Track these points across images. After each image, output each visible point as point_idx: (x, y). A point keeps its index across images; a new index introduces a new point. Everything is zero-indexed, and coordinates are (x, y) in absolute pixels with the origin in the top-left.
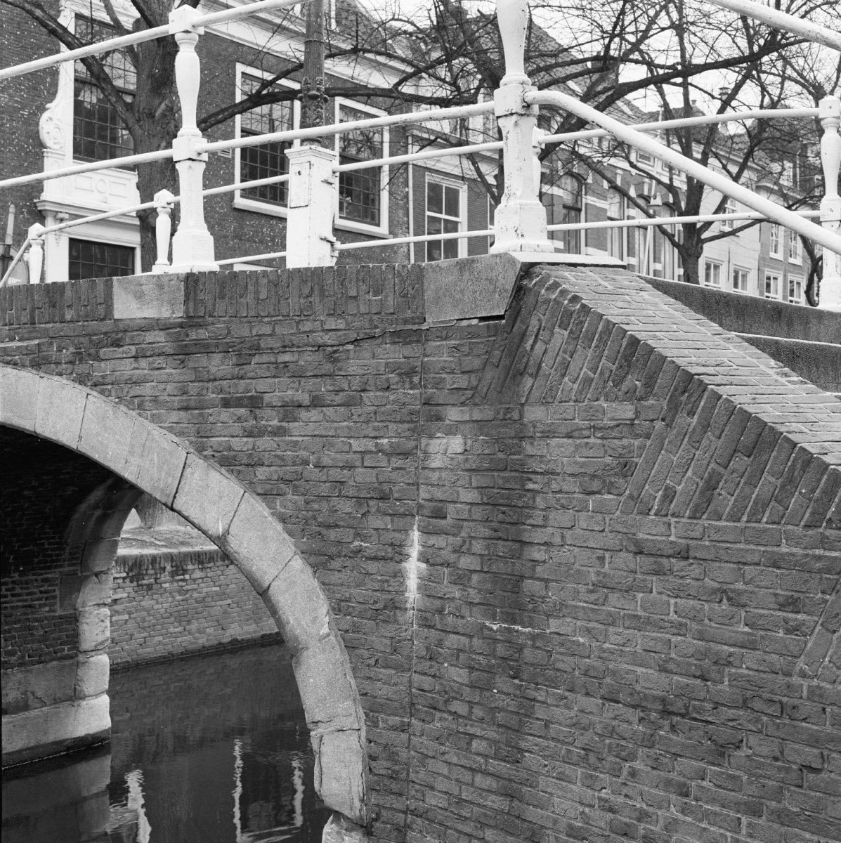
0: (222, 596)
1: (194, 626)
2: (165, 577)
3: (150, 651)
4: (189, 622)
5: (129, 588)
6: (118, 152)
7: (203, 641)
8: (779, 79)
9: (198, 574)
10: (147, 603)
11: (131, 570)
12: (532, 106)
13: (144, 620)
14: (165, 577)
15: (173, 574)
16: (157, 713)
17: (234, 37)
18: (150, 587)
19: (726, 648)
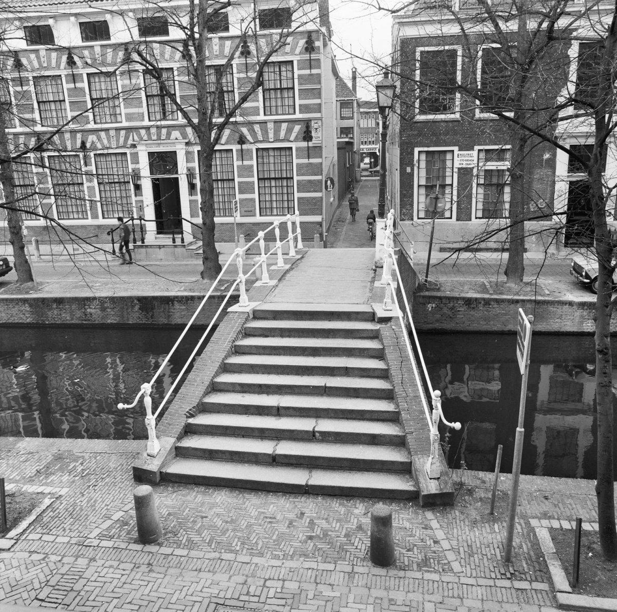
0: (505, 314)
1: (492, 323)
2: (481, 305)
3: (471, 328)
4: (489, 321)
5: (465, 307)
6: (169, 363)
7: (495, 328)
8: (265, 589)
9: (496, 306)
10: (472, 313)
11: (466, 301)
12: (505, 276)
13: (470, 318)
14: (481, 305)
15: (484, 305)
16: (257, 513)
17: (199, 353)
18: (473, 308)
19: (423, 19)
